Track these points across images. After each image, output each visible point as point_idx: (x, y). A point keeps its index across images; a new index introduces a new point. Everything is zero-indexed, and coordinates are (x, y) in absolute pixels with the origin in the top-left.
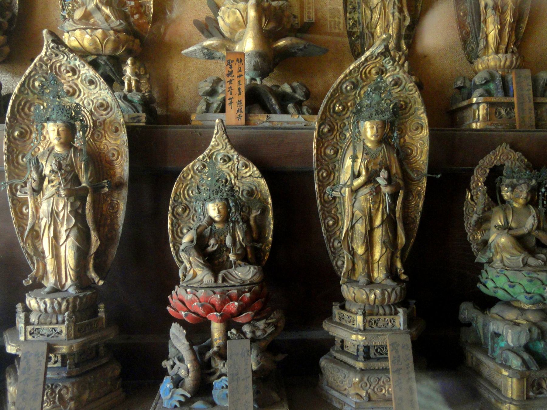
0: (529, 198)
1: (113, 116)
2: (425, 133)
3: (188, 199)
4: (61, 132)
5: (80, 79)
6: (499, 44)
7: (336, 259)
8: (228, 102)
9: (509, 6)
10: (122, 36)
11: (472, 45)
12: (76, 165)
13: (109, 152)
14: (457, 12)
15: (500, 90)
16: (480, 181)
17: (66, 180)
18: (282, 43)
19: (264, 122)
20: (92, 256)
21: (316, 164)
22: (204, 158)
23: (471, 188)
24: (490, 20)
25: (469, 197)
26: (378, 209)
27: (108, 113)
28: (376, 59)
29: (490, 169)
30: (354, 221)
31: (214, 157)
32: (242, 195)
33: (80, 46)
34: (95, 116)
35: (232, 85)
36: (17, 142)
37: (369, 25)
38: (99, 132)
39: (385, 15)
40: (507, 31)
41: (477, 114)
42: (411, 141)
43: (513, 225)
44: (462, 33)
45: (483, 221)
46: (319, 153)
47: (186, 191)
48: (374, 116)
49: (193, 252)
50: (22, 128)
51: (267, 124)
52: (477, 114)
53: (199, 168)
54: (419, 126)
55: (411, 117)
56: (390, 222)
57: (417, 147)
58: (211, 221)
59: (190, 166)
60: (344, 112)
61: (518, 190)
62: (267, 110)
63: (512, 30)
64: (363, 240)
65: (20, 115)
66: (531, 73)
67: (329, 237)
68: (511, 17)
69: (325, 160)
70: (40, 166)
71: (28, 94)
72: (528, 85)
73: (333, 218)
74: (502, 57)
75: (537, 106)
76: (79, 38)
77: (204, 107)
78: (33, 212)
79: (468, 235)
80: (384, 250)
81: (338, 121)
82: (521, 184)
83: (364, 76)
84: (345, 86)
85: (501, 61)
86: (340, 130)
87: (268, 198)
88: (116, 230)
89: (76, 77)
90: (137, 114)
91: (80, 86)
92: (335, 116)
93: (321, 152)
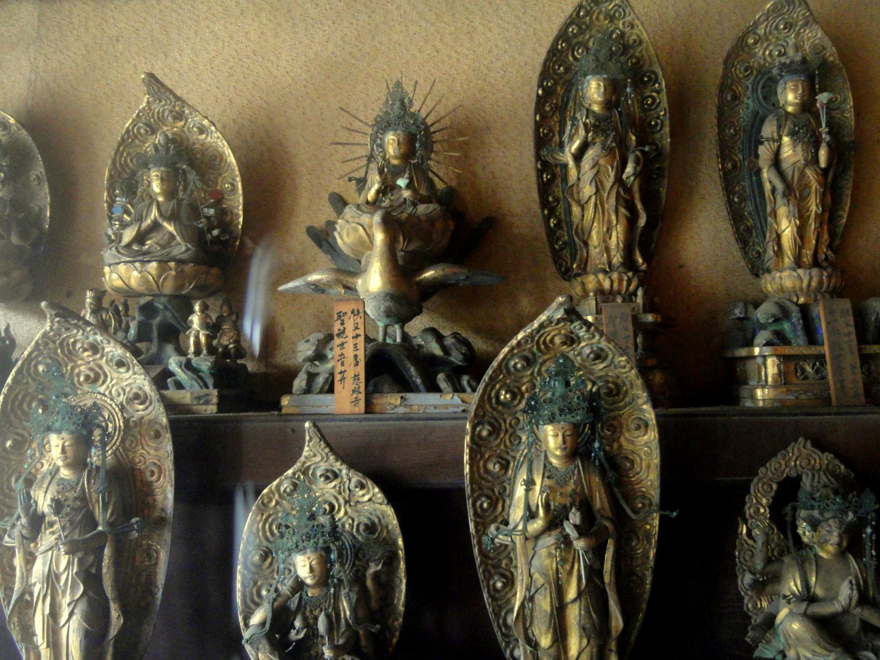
0: (845, 544)
1: (153, 413)
2: (652, 436)
3: (271, 539)
4: (67, 448)
5: (105, 359)
6: (801, 248)
7: (511, 646)
8: (338, 377)
9: (814, 188)
10: (189, 268)
11: (758, 248)
12: (90, 497)
13: (146, 468)
14: (728, 197)
15: (800, 333)
16: (761, 505)
17: (71, 522)
18: (429, 274)
19: (396, 407)
20: (112, 642)
21: (469, 489)
22: (294, 474)
23: (747, 516)
24: (782, 211)
25: (745, 531)
26: (570, 572)
27: (147, 408)
28: (557, 324)
29: (779, 484)
30: (533, 590)
31: (310, 473)
32: (358, 531)
33: (125, 287)
34: (127, 412)
35: (344, 351)
36: (10, 456)
37: (580, 228)
38: (133, 436)
39: (603, 213)
40: (813, 227)
41: (763, 373)
42: (631, 447)
43: (819, 592)
44: (738, 230)
45: (767, 582)
46: (475, 469)
47: (267, 526)
48: (557, 417)
49: (264, 645)
50: (18, 434)
51: (401, 410)
52: (763, 373)
53: (288, 490)
54: (641, 423)
55: (627, 408)
56: (594, 593)
57: (641, 458)
58: (299, 585)
59: (273, 488)
60: (516, 402)
61: (823, 530)
62: (405, 386)
63: (821, 224)
64: (547, 623)
65: (16, 416)
66: (852, 303)
67: (497, 609)
68: (817, 206)
69: (487, 481)
70: (31, 506)
71: (27, 383)
72: (847, 325)
73: (503, 576)
74: (804, 275)
75: (865, 359)
76: (124, 276)
77: (304, 384)
78: (22, 574)
79: (746, 601)
80: (585, 641)
81: (505, 416)
82: (828, 519)
83: (543, 347)
84: (513, 363)
85: (802, 282)
86: (510, 431)
87: (397, 539)
88: (153, 594)
89: (98, 356)
90: (205, 391)
91: (106, 369)
92: (500, 408)
93: (478, 469)
